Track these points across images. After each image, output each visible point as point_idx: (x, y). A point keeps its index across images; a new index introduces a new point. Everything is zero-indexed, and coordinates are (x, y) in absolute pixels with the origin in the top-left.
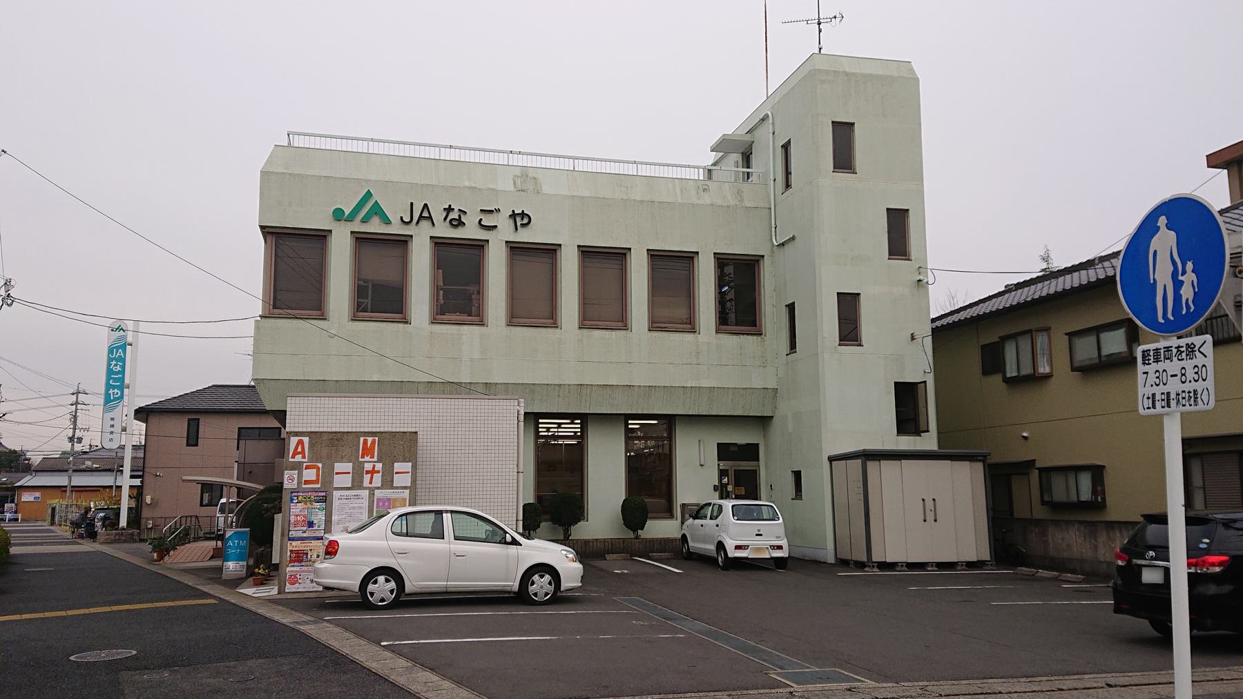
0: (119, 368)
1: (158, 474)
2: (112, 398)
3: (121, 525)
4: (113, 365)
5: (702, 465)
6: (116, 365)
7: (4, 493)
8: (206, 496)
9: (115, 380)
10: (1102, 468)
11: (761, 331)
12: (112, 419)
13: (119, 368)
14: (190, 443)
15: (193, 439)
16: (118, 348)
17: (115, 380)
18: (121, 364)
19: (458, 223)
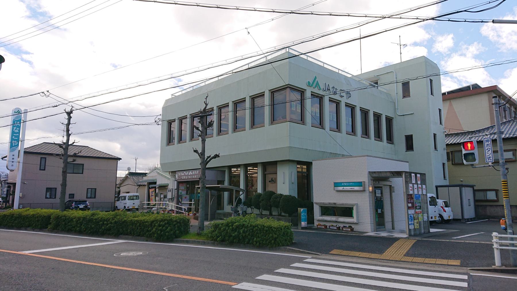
0: (17, 131)
1: (25, 183)
2: (13, 145)
3: (430, 229)
4: (14, 129)
5: (293, 183)
6: (16, 129)
7: (516, 221)
8: (48, 194)
9: (15, 137)
10: (498, 190)
11: (393, 143)
12: (13, 155)
13: (17, 131)
14: (41, 169)
15: (43, 168)
16: (17, 121)
17: (15, 137)
18: (18, 129)
19: (335, 93)
